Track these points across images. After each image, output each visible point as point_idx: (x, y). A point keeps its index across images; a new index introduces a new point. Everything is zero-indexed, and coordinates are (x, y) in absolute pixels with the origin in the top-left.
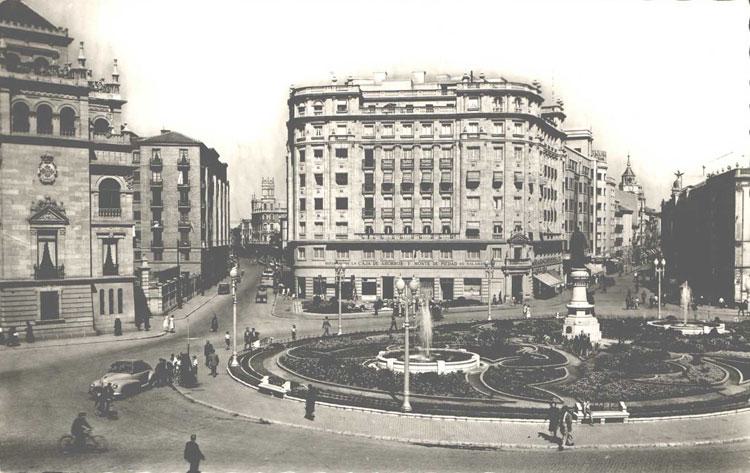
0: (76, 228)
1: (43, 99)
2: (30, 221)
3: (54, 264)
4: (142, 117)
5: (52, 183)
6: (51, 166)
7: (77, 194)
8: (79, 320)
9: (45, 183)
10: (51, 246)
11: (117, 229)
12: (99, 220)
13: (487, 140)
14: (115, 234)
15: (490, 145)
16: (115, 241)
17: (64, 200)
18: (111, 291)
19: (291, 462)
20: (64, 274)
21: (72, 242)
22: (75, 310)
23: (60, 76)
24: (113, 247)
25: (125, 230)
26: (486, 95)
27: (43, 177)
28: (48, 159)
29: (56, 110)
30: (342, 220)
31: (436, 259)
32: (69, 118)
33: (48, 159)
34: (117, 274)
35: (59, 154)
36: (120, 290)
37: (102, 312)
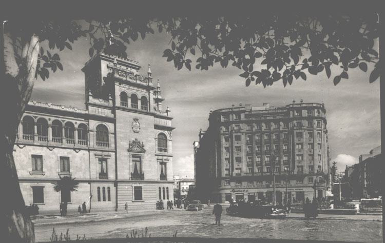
0: (149, 156)
1: (133, 91)
2: (128, 151)
3: (139, 173)
4: (126, 51)
5: (138, 132)
6: (137, 123)
7: (149, 139)
8: (151, 201)
9: (135, 132)
10: (138, 164)
11: (106, 153)
12: (158, 153)
13: (305, 129)
14: (105, 156)
15: (306, 131)
16: (106, 160)
17: (142, 141)
18: (164, 188)
19: (233, 225)
20: (144, 178)
21: (147, 162)
22: (149, 197)
23: (140, 81)
24: (104, 164)
25: (169, 158)
26: (304, 109)
27: (134, 129)
28: (136, 120)
29: (139, 97)
30: (239, 167)
31: (282, 184)
32: (145, 101)
33: (136, 120)
34: (167, 180)
35: (141, 119)
36: (167, 188)
37: (164, 199)
